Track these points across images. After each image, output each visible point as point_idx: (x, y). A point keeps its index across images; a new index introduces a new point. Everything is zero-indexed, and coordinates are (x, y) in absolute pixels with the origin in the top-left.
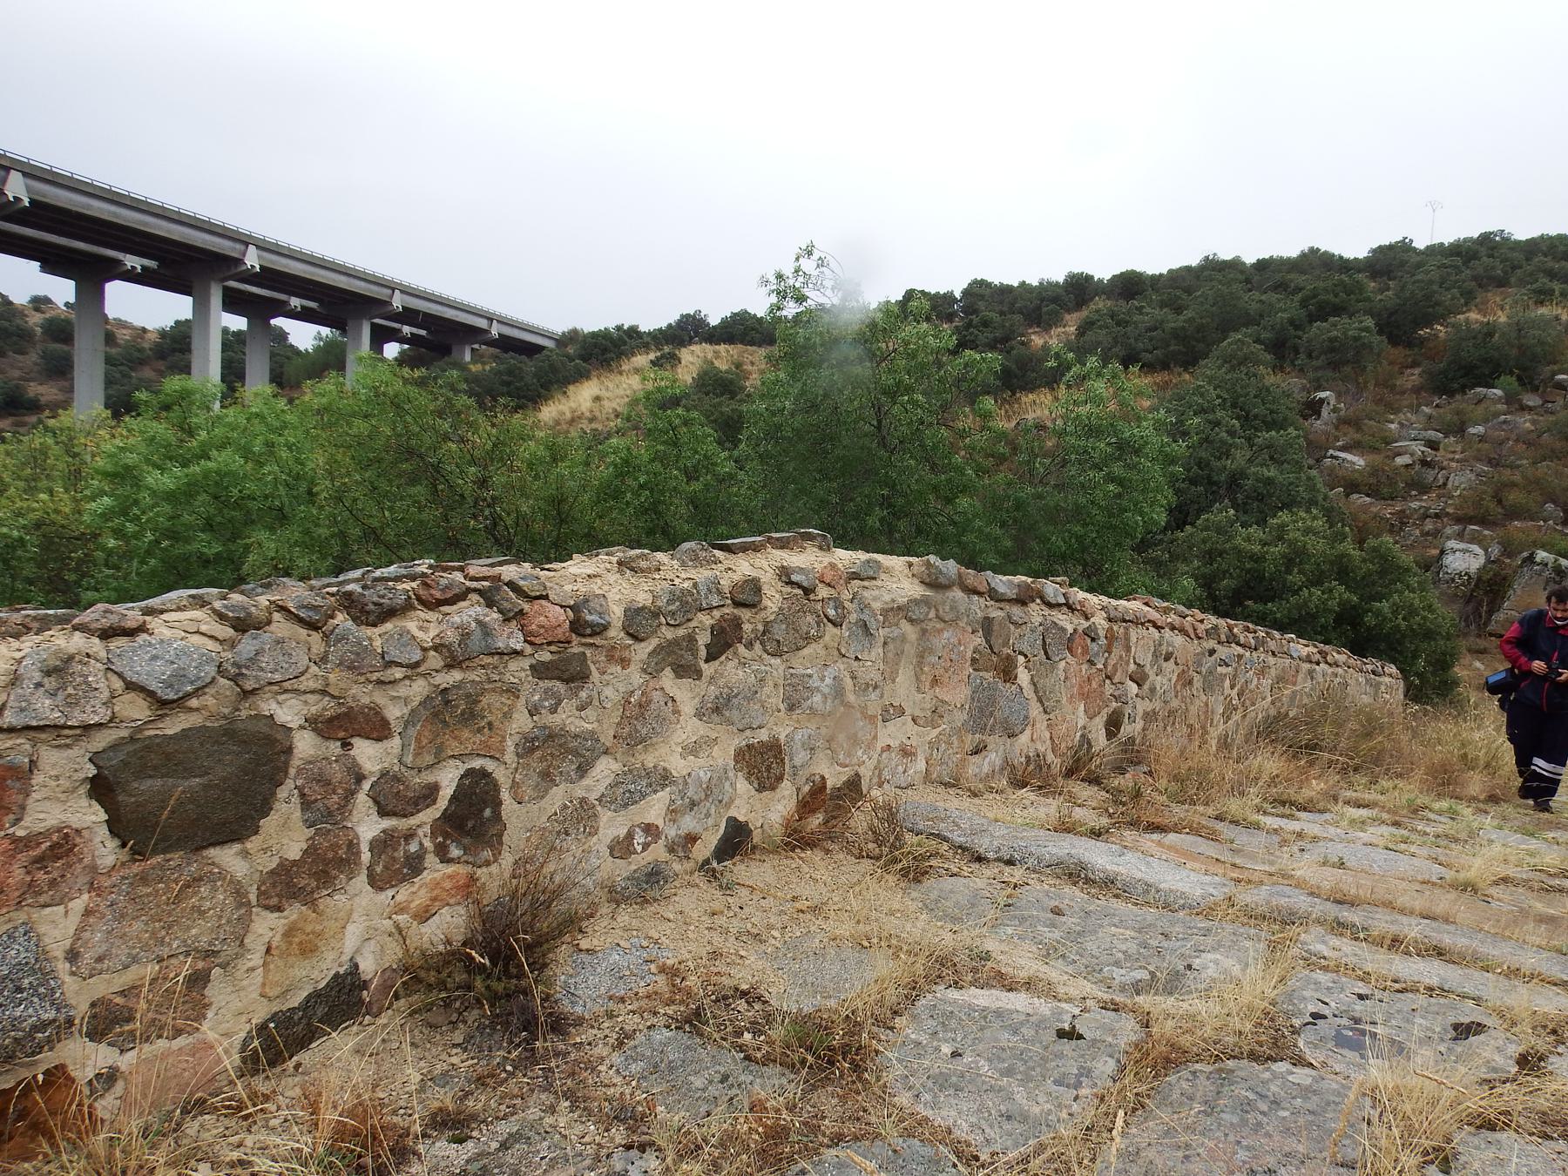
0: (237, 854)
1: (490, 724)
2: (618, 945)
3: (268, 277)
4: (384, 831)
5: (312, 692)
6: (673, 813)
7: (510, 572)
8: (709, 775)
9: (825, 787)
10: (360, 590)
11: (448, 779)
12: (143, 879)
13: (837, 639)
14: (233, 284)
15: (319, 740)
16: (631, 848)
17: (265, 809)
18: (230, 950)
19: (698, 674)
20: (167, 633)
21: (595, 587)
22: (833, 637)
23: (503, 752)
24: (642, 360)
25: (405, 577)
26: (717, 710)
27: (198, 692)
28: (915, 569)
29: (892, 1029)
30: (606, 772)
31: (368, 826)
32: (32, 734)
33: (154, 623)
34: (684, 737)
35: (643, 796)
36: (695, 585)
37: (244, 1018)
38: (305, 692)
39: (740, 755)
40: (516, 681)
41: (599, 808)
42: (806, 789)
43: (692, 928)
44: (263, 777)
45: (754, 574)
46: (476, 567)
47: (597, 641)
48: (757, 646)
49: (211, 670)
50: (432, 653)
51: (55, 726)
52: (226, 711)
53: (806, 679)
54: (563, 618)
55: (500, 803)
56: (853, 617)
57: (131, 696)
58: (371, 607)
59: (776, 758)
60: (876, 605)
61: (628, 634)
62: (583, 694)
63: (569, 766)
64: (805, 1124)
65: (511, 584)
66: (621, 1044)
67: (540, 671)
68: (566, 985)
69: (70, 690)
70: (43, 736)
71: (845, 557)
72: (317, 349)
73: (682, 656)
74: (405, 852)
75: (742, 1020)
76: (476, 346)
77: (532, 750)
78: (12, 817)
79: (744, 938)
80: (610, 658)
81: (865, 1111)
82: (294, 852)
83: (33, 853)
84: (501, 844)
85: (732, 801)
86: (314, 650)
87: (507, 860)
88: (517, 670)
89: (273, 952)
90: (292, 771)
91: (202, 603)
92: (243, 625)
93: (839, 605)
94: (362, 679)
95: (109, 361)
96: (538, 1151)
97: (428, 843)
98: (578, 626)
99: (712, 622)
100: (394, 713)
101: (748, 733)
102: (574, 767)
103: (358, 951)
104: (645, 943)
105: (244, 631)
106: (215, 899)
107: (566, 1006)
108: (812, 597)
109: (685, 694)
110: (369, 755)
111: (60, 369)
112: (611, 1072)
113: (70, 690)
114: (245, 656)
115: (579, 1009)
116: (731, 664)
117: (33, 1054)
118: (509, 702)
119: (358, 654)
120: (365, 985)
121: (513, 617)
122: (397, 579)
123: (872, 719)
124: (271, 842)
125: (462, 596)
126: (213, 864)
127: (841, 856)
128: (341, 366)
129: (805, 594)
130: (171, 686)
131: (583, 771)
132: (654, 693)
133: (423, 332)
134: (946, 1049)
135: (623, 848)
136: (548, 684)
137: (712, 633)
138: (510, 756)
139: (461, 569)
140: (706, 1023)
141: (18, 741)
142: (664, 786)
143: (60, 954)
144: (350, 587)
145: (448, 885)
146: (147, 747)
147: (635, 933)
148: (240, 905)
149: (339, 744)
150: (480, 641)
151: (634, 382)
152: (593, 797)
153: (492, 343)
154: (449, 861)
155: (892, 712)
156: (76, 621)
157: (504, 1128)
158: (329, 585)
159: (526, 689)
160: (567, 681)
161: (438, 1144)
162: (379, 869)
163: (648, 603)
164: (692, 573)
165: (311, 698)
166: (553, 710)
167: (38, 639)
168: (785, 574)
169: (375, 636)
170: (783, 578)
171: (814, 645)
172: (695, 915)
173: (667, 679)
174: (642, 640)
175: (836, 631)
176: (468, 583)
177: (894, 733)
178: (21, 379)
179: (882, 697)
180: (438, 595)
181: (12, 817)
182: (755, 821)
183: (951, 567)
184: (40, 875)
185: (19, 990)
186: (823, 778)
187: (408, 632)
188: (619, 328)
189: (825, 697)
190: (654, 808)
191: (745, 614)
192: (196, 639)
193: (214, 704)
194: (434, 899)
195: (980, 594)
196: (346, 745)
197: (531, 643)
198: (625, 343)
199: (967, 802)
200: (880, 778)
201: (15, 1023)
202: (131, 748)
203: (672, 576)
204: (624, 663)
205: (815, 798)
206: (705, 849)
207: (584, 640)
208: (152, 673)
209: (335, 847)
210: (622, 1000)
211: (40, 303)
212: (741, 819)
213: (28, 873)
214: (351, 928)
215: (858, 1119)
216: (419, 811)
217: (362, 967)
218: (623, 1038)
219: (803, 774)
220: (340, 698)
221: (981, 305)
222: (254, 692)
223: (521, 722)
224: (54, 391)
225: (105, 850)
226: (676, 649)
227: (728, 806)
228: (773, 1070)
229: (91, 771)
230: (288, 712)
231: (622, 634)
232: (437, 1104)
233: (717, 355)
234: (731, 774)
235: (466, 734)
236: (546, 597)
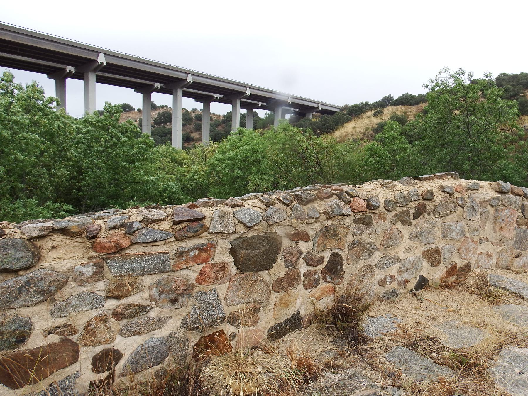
0: (267, 274)
1: (340, 238)
2: (382, 316)
3: (253, 97)
4: (308, 271)
5: (288, 226)
6: (400, 272)
7: (346, 188)
8: (413, 259)
9: (456, 266)
10: (300, 194)
11: (327, 255)
12: (242, 279)
13: (462, 212)
14: (243, 100)
15: (289, 241)
16: (386, 283)
17: (274, 261)
18: (265, 303)
19: (410, 224)
20: (248, 206)
21: (374, 193)
22: (461, 211)
23: (344, 248)
24: (370, 113)
25: (313, 189)
26: (417, 237)
27: (257, 224)
28: (493, 186)
29: (492, 359)
30: (378, 256)
31: (303, 269)
32: (216, 235)
33: (245, 203)
35: (390, 265)
36: (409, 192)
37: (268, 324)
38: (286, 226)
39: (424, 253)
40: (349, 224)
41: (375, 268)
42: (450, 267)
43: (409, 313)
44: (274, 251)
45: (430, 189)
46: (335, 186)
47: (375, 211)
48: (432, 214)
49: (260, 218)
50: (323, 214)
51: (222, 233)
52: (264, 230)
53: (450, 227)
54: (364, 204)
55: (343, 265)
56: (469, 204)
57: (240, 225)
58: (304, 199)
59: (438, 254)
60: (478, 200)
61: (386, 209)
62: (370, 230)
63: (365, 254)
64: (461, 390)
65: (346, 192)
66: (387, 350)
67: (356, 221)
68: (365, 327)
69: (225, 223)
70: (219, 235)
71: (464, 182)
72: (266, 117)
73: (404, 217)
74: (314, 278)
75: (432, 348)
76: (314, 113)
77: (354, 248)
78: (211, 258)
79: (429, 319)
80: (380, 218)
81: (485, 389)
82: (282, 275)
83: (217, 269)
84: (343, 278)
85: (421, 269)
86: (288, 213)
87: (345, 283)
88: (349, 221)
89: (276, 305)
90: (282, 250)
91: (256, 197)
92: (268, 204)
93: (463, 199)
94: (302, 222)
95: (211, 125)
96: (362, 382)
97: (321, 276)
98: (369, 206)
99: (415, 205)
100: (311, 233)
101: (428, 245)
102: (367, 254)
103: (300, 308)
104: (392, 316)
105: (268, 206)
106: (260, 286)
107: (366, 334)
108: (452, 197)
109: (406, 231)
110: (304, 246)
111: (199, 129)
112: (384, 359)
113: (225, 223)
114: (269, 214)
115: (371, 336)
116: (422, 221)
117: (216, 326)
118: (346, 231)
119: (301, 214)
120: (301, 318)
121: (348, 203)
122: (311, 190)
123: (475, 242)
124: (276, 271)
125: (331, 196)
126: (260, 276)
127: (464, 292)
128: (273, 123)
129: (450, 196)
130: (250, 222)
131: (370, 255)
132: (395, 230)
134: (517, 370)
135: (382, 283)
136: (359, 226)
137: (415, 209)
138: (346, 249)
139: (330, 187)
140: (418, 347)
141: (213, 237)
142: (397, 262)
143: (222, 298)
144: (298, 193)
145: (327, 290)
146: (244, 240)
147: (388, 312)
148: (268, 290)
149: (295, 242)
150: (337, 211)
151: (367, 121)
152: (373, 264)
153: (319, 112)
154: (327, 282)
155: (483, 240)
156: (225, 202)
157: (350, 372)
158: (291, 192)
159: (352, 227)
160: (365, 225)
161: (328, 373)
162: (306, 282)
163: (393, 199)
164: (407, 188)
165: (287, 227)
166: (361, 235)
167: (216, 207)
168: (442, 189)
169: (306, 209)
170: (441, 190)
171: (453, 214)
172: (409, 308)
173: (399, 225)
174: (390, 212)
175: (462, 209)
176: (333, 192)
177: (483, 248)
178: (190, 132)
179: (479, 234)
180: (324, 195)
181: (211, 258)
182: (429, 277)
183: (508, 185)
184: (218, 275)
185: (213, 307)
186: (456, 263)
187: (315, 207)
188: (362, 103)
189: (457, 234)
190: (394, 270)
191: (427, 203)
192: (256, 208)
193: (261, 228)
194: (322, 294)
195: (520, 195)
196: (297, 243)
197: (354, 212)
198: (364, 108)
199: (515, 276)
200: (478, 265)
201: (213, 316)
202: (240, 240)
203: (400, 189)
204: (384, 219)
205: (452, 270)
206: (412, 285)
207: (371, 211)
208: (245, 218)
209: (294, 274)
210: (386, 335)
211: (194, 110)
212: (425, 276)
213: (215, 274)
214: (298, 300)
215: (482, 391)
216: (318, 265)
217: (301, 313)
218: (387, 349)
219: (448, 261)
220: (296, 228)
221: (504, 83)
222: (271, 225)
223: (350, 238)
224: (197, 135)
225: (233, 270)
226: (402, 215)
227: (420, 271)
228: (444, 368)
229: (230, 247)
230: (279, 231)
231: (384, 209)
232: (327, 360)
233: (397, 109)
234: (421, 260)
235: (333, 241)
236: (358, 197)
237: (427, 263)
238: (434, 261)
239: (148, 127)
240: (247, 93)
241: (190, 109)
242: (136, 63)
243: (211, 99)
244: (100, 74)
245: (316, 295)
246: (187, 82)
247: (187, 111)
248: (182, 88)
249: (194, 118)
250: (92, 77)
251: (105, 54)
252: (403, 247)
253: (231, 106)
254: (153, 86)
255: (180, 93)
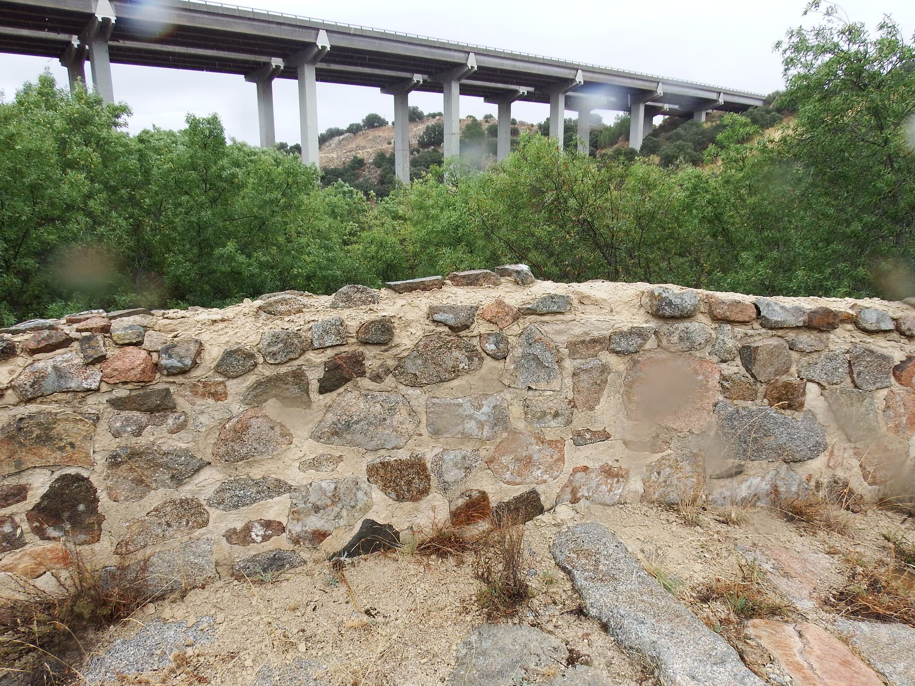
6: (295, 513)
26: (336, 433)
34: (301, 454)
39: (372, 471)
55: (96, 500)
59: (418, 473)
67: (118, 404)
72: (617, 125)
76: (710, 111)
93: (501, 339)
101: (383, 452)
133: (676, 107)
211: (488, 118)
216: (9, 505)
234: (364, 485)
237: (381, 493)
238: (405, 488)
239: (405, 152)
240: (578, 80)
241: (480, 118)
242: (380, 42)
243: (512, 96)
244: (323, 66)
245: (20, 567)
246: (467, 69)
247: (475, 120)
248: (459, 79)
249: (486, 132)
250: (309, 73)
251: (327, 31)
252: (296, 457)
253: (547, 106)
254: (411, 79)
255: (455, 88)
